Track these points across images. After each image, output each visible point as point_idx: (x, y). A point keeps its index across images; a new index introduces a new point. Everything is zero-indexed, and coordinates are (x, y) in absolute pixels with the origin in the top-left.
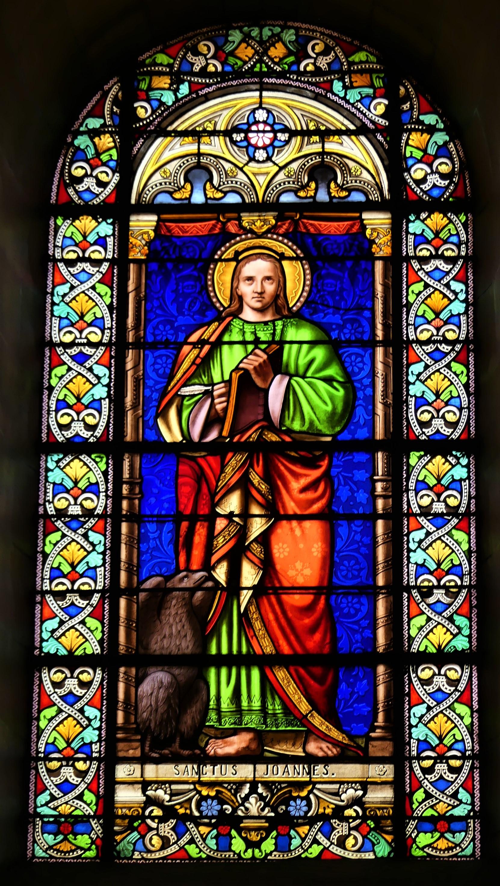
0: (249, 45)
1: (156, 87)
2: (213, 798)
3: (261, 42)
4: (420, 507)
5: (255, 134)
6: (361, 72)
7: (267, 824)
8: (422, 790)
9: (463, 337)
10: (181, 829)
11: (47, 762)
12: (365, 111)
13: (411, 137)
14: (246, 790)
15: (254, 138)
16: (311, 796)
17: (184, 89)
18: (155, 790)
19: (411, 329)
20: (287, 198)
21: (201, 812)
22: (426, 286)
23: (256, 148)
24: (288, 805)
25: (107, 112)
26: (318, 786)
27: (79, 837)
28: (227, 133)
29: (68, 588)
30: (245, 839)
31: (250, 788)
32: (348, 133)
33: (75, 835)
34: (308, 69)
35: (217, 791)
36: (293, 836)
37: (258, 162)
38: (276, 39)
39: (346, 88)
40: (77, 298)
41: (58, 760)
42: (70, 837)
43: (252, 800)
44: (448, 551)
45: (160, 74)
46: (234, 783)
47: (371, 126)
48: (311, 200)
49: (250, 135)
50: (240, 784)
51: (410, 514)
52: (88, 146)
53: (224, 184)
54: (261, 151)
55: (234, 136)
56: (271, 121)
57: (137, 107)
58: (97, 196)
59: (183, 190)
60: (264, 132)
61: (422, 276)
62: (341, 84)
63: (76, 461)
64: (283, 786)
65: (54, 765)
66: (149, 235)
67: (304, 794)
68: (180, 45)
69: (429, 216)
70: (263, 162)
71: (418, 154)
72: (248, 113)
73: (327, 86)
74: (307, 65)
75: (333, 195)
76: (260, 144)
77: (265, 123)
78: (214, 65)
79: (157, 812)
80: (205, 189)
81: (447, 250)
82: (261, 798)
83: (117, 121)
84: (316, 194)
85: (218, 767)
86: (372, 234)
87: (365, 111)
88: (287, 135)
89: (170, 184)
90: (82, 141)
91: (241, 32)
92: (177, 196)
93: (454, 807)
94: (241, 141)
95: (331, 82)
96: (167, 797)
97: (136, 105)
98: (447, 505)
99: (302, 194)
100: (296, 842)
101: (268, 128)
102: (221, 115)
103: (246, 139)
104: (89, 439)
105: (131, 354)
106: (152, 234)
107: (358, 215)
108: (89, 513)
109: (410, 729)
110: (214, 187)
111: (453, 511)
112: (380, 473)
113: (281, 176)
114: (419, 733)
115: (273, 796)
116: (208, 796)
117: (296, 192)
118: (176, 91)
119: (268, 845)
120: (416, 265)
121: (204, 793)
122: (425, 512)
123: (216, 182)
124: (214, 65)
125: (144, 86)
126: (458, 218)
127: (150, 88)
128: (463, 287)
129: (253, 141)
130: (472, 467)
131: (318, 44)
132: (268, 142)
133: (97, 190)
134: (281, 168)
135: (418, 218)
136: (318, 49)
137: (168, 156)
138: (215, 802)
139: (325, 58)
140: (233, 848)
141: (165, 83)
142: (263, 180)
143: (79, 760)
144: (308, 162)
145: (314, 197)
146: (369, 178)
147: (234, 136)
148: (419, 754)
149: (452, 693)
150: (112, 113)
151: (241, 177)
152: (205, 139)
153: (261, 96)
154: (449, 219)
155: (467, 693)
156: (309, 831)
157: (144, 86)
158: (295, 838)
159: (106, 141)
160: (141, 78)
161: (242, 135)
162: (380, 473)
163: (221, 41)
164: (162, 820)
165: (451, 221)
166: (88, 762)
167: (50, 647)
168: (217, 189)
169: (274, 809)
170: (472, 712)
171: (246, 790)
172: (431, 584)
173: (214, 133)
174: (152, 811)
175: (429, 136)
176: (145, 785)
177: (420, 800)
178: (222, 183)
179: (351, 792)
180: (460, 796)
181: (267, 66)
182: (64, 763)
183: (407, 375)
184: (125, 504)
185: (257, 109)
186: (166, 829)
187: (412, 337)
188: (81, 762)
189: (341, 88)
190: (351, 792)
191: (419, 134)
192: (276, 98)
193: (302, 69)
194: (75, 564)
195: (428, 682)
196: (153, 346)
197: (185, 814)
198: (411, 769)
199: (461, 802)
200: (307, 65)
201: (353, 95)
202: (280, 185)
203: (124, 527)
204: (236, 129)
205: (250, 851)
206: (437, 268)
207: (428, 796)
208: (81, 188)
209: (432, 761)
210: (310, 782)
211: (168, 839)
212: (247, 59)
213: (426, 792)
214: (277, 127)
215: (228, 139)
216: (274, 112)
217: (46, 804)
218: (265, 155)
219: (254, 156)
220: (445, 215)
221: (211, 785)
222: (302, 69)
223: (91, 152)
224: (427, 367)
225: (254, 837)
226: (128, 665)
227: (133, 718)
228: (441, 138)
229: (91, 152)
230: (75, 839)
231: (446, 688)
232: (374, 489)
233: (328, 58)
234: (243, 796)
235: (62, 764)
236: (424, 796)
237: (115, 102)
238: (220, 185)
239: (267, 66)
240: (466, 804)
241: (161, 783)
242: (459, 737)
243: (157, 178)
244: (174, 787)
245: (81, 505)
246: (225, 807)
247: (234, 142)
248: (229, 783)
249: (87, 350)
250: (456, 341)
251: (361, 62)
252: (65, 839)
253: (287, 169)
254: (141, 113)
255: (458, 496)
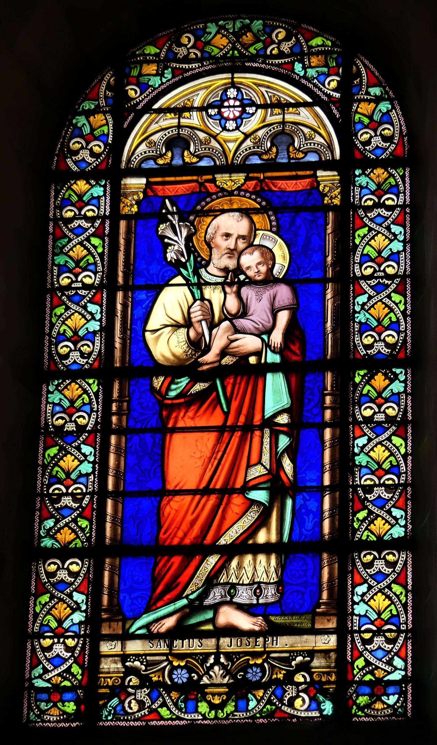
0: (223, 36)
1: (145, 73)
2: (182, 668)
3: (234, 33)
4: (363, 417)
5: (227, 109)
6: (318, 53)
7: (227, 690)
8: (362, 658)
9: (401, 272)
10: (155, 695)
11: (41, 640)
12: (321, 87)
13: (360, 106)
14: (211, 660)
15: (226, 113)
16: (266, 664)
17: (168, 74)
18: (133, 662)
19: (357, 267)
20: (151, 164)
21: (171, 679)
22: (370, 229)
23: (227, 119)
24: (247, 672)
25: (102, 95)
26: (273, 655)
27: (66, 704)
28: (201, 109)
29: (63, 492)
30: (209, 703)
31: (214, 659)
32: (305, 104)
33: (63, 702)
34: (274, 52)
35: (187, 662)
36: (250, 699)
37: (229, 130)
38: (247, 28)
39: (304, 68)
40: (74, 249)
41: (50, 637)
42: (59, 705)
43: (216, 668)
44: (387, 453)
45: (149, 62)
46: (201, 654)
47: (325, 98)
48: (273, 162)
49: (223, 110)
50: (207, 655)
51: (356, 423)
52: (84, 124)
53: (199, 151)
54: (231, 122)
55: (210, 111)
56: (240, 97)
57: (128, 90)
58: (90, 164)
59: (165, 157)
60: (234, 106)
61: (367, 222)
62: (301, 65)
63: (73, 384)
64: (241, 655)
65: (47, 642)
66: (138, 196)
67: (259, 661)
68: (165, 39)
69: (372, 171)
70: (233, 130)
71: (366, 121)
72: (220, 93)
73: (289, 66)
74: (273, 49)
75: (291, 157)
76: (231, 116)
77: (235, 99)
78: (195, 54)
79: (135, 681)
80: (183, 156)
81: (388, 199)
82: (223, 667)
83: (111, 101)
84: (276, 156)
85: (186, 642)
86: (324, 188)
87: (321, 87)
88: (254, 108)
89: (153, 152)
90: (81, 120)
91: (217, 25)
92: (161, 162)
93: (389, 673)
94: (215, 115)
95: (293, 63)
96: (143, 667)
97: (127, 88)
98: (386, 415)
99: (265, 157)
100: (252, 704)
101: (238, 103)
102: (199, 94)
103: (220, 113)
104: (84, 365)
105: (120, 295)
106: (141, 196)
107: (210, 177)
108: (81, 429)
109: (352, 606)
110: (191, 153)
111: (390, 420)
112: (329, 388)
113: (248, 143)
114: (360, 609)
115: (233, 663)
116: (179, 666)
117: (260, 155)
118: (162, 75)
119: (230, 708)
120: (361, 212)
121: (175, 664)
122: (368, 420)
123: (296, 144)
124: (195, 54)
125: (135, 73)
126: (397, 172)
127: (140, 75)
128: (402, 229)
129: (226, 115)
130: (409, 383)
131: (280, 32)
132: (237, 114)
133: (90, 159)
134: (247, 136)
135: (363, 173)
136: (281, 36)
137: (154, 127)
138: (184, 671)
139: (287, 43)
140: (200, 710)
141: (153, 70)
142: (232, 146)
143: (68, 637)
144: (270, 130)
145: (169, 164)
146: (322, 141)
147: (210, 111)
148: (360, 627)
149: (391, 573)
150: (106, 97)
151: (214, 143)
152: (187, 114)
153: (233, 78)
154: (388, 172)
155: (403, 575)
156: (264, 694)
157: (135, 73)
158: (252, 700)
159: (99, 119)
160: (133, 66)
161: (216, 110)
162: (329, 388)
163: (200, 33)
164: (140, 687)
165: (391, 175)
166: (76, 640)
167: (48, 543)
168: (193, 155)
169: (233, 676)
170: (407, 591)
171: (211, 660)
172: (372, 483)
173: (191, 109)
174: (130, 680)
175: (375, 105)
176: (124, 658)
177: (360, 667)
178: (197, 150)
179: (299, 659)
180: (395, 663)
181: (239, 52)
182: (56, 640)
183: (354, 305)
184: (114, 419)
185: (229, 88)
186: (142, 694)
187: (358, 274)
188: (70, 640)
189: (301, 69)
190: (299, 659)
191: (366, 104)
192: (245, 78)
193: (268, 53)
194: (71, 471)
195: (370, 565)
196: (135, 288)
197: (159, 681)
198: (353, 641)
199: (396, 669)
200: (273, 49)
201: (311, 72)
202: (141, 154)
203: (113, 439)
204: (211, 106)
205: (213, 712)
206: (379, 215)
207: (368, 663)
208: (79, 157)
209: (371, 634)
210: (264, 652)
211: (144, 703)
212: (222, 47)
213: (366, 660)
214: (246, 102)
215: (204, 113)
216: (243, 91)
217: (40, 677)
218: (235, 125)
219: (225, 127)
220: (386, 170)
221: (181, 657)
222: (268, 53)
223: (87, 130)
224: (370, 298)
225: (217, 701)
226: (112, 557)
227: (115, 600)
228: (384, 106)
229: (87, 130)
230: (64, 706)
231: (385, 570)
232: (324, 402)
233: (290, 43)
234: (208, 665)
235: (54, 641)
236: (364, 663)
237: (109, 87)
238: (195, 152)
239: (239, 52)
240: (400, 669)
241: (137, 656)
242: (395, 612)
243: (143, 147)
244: (148, 658)
245: (75, 422)
246: (193, 675)
247: (210, 116)
248: (196, 654)
249: (82, 292)
250: (395, 276)
251: (318, 46)
252: (55, 705)
253: (252, 136)
254: (132, 94)
255: (396, 408)
